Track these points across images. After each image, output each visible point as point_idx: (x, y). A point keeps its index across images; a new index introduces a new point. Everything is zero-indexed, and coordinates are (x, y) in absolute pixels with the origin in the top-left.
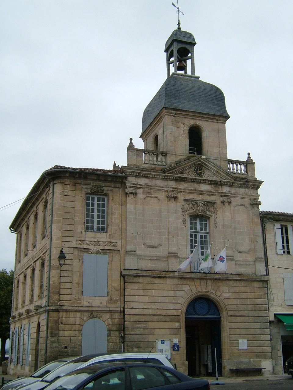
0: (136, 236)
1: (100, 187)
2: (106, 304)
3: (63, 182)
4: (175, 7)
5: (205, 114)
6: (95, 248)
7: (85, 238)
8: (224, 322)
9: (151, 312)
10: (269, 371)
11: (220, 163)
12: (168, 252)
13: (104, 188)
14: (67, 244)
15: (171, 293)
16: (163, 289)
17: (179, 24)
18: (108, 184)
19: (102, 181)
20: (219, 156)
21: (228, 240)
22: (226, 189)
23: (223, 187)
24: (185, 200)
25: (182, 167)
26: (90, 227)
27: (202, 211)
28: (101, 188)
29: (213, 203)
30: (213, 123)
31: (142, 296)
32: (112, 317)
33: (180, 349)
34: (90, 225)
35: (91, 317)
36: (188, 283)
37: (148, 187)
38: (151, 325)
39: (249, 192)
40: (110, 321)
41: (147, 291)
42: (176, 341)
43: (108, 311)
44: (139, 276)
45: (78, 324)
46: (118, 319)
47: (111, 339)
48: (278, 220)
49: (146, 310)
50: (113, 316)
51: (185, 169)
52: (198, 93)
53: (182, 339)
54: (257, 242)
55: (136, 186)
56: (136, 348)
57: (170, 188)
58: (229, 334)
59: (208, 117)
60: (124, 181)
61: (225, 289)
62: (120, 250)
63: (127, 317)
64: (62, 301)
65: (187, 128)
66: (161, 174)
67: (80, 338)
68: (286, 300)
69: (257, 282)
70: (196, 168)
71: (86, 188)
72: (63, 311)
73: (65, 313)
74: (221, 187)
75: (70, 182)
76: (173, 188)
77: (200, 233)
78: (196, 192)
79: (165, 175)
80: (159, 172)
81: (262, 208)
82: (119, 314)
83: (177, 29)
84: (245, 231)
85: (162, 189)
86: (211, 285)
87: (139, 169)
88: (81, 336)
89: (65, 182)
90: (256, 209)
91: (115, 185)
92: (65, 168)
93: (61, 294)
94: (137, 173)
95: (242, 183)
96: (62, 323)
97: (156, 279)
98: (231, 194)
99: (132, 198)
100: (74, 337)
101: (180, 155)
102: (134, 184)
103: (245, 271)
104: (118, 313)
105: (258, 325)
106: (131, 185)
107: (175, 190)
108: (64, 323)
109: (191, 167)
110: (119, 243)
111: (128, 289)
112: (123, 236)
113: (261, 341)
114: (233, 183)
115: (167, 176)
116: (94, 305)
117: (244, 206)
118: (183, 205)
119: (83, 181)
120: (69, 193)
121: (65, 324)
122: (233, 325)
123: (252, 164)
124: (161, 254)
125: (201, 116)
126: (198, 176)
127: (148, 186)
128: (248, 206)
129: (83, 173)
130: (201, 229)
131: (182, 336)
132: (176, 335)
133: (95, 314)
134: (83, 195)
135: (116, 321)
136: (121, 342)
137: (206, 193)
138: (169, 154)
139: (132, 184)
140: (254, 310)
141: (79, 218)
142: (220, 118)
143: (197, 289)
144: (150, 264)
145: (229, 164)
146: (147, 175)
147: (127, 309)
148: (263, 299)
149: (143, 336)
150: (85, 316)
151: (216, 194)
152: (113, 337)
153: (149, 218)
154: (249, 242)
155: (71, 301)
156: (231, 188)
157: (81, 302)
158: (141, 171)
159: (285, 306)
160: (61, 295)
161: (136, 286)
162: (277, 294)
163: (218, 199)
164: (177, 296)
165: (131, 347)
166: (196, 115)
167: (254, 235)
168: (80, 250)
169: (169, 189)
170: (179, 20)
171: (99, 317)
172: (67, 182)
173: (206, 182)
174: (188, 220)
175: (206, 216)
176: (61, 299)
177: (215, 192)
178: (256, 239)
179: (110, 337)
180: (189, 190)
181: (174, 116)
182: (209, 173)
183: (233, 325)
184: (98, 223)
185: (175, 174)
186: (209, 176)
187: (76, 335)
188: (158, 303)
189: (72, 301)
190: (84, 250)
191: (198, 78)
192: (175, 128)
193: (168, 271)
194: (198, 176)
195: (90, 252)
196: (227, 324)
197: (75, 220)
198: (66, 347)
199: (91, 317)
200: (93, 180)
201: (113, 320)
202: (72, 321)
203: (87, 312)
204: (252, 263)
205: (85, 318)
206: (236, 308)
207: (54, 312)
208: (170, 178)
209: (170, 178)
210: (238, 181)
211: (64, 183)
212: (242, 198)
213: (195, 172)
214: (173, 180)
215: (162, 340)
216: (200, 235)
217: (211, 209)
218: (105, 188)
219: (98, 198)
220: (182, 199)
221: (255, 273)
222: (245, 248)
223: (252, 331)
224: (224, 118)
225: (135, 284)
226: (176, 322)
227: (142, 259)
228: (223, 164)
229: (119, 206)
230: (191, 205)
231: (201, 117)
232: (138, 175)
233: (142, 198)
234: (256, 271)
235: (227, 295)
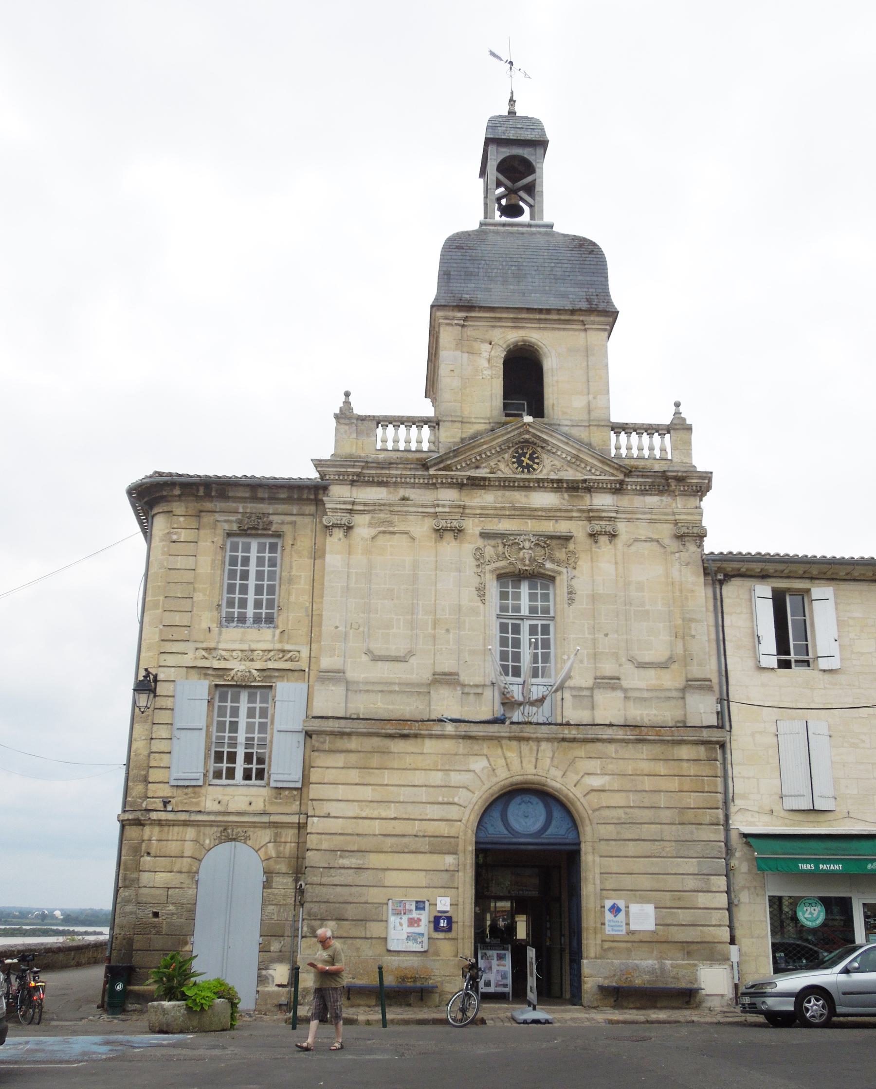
0: (346, 634)
1: (261, 515)
2: (265, 806)
3: (170, 509)
4: (501, 60)
5: (548, 311)
6: (242, 668)
7: (218, 642)
8: (585, 854)
9: (377, 827)
10: (722, 996)
11: (590, 434)
12: (432, 672)
13: (271, 518)
14: (171, 660)
15: (437, 778)
16: (413, 766)
17: (512, 101)
18: (281, 508)
19: (266, 501)
20: (585, 417)
21: (606, 635)
22: (603, 501)
23: (594, 494)
24: (484, 535)
25: (476, 450)
26: (236, 616)
27: (532, 560)
28: (265, 519)
29: (567, 539)
30: (571, 333)
31: (356, 784)
32: (278, 840)
33: (454, 926)
34: (236, 610)
35: (223, 838)
36: (485, 751)
37: (382, 508)
38: (374, 860)
39: (674, 505)
40: (271, 850)
41: (369, 772)
42: (443, 904)
43: (266, 823)
44: (349, 734)
45: (189, 855)
46: (293, 844)
47: (273, 894)
48: (763, 576)
49: (365, 821)
50: (281, 838)
51: (486, 455)
52: (532, 260)
53: (461, 900)
54: (694, 637)
55: (350, 507)
56: (331, 920)
57: (444, 506)
58: (598, 888)
59: (556, 317)
60: (320, 497)
61: (594, 765)
62: (307, 670)
63: (312, 841)
64: (153, 797)
65: (500, 355)
66: (417, 473)
67: (190, 892)
68: (786, 796)
69: (689, 746)
70: (517, 452)
71: (226, 521)
72: (151, 824)
73: (157, 829)
74: (588, 495)
75: (187, 508)
76: (451, 507)
77: (528, 618)
78: (517, 513)
79: (429, 475)
80: (411, 469)
81: (713, 545)
82: (296, 831)
83: (507, 114)
84: (660, 608)
85: (420, 510)
86: (551, 755)
87: (357, 464)
88: (195, 887)
89: (174, 510)
90: (692, 548)
91: (301, 508)
92: (170, 475)
93: (150, 782)
94: (354, 474)
95: (649, 480)
96: (149, 854)
97: (396, 740)
98: (617, 512)
99: (340, 539)
100: (178, 890)
101: (475, 423)
102: (345, 503)
103: (655, 715)
104: (292, 828)
105: (691, 866)
106: (339, 506)
107: (457, 510)
108: (153, 853)
109: (502, 450)
110: (305, 653)
111: (318, 767)
112: (315, 635)
113: (700, 911)
114: (621, 483)
115: (436, 477)
116: (232, 808)
117: (658, 541)
118: (478, 549)
119: (220, 505)
120: (184, 535)
121: (155, 857)
122: (614, 865)
123: (684, 429)
124: (414, 677)
125: (538, 316)
126: (523, 471)
127: (384, 505)
128: (667, 541)
129: (214, 485)
130: (533, 610)
131: (461, 890)
132: (445, 888)
133: (233, 831)
134: (219, 540)
135: (289, 849)
136: (298, 903)
137: (544, 514)
138: (444, 421)
139: (340, 503)
140: (680, 824)
141: (205, 595)
142: (592, 318)
143: (509, 765)
144: (379, 704)
145: (618, 434)
146: (380, 479)
147: (314, 818)
148: (707, 792)
149: (354, 889)
150: (209, 836)
151: (575, 514)
152: (276, 891)
153: (383, 586)
154: (668, 638)
155: (174, 797)
156: (620, 497)
157: (200, 801)
158: (363, 468)
159: (783, 814)
160: (150, 785)
161: (339, 760)
162: (758, 780)
163: (578, 529)
164: (452, 785)
165: (319, 917)
166: (524, 316)
167: (684, 620)
168: (204, 671)
169: (438, 509)
170: (512, 93)
171: (243, 838)
172: (179, 508)
173: (543, 487)
174: (493, 589)
175: (544, 574)
176: (150, 794)
177: (571, 511)
178: (690, 628)
179: (269, 891)
180: (495, 508)
181: (463, 326)
182: (556, 462)
183: (614, 865)
184: (258, 604)
185: (457, 470)
186: (555, 470)
187: (181, 883)
188: (397, 802)
189: (176, 799)
190: (214, 673)
191: (551, 226)
192: (466, 355)
193: (429, 720)
194: (523, 471)
195: (230, 678)
196: (594, 861)
197: (195, 599)
198: (156, 915)
199: (223, 838)
200: (243, 499)
201: (280, 846)
202: (173, 847)
203: (211, 826)
204: (675, 694)
205: (207, 842)
206: (623, 816)
207: (133, 825)
208: (442, 483)
209: (442, 483)
210: (638, 476)
211: (172, 512)
212: (652, 521)
213: (514, 463)
214: (451, 485)
215: (417, 902)
216: (530, 625)
217: (560, 555)
218: (275, 519)
219: (259, 543)
220: (478, 533)
221: (684, 722)
222: (658, 651)
223: (673, 883)
224: (601, 316)
225: (338, 755)
226: (445, 853)
227: (360, 691)
228: (596, 437)
229: (309, 560)
230: (500, 548)
231: (535, 321)
232: (356, 481)
233: (366, 536)
234: (685, 715)
235: (596, 782)
